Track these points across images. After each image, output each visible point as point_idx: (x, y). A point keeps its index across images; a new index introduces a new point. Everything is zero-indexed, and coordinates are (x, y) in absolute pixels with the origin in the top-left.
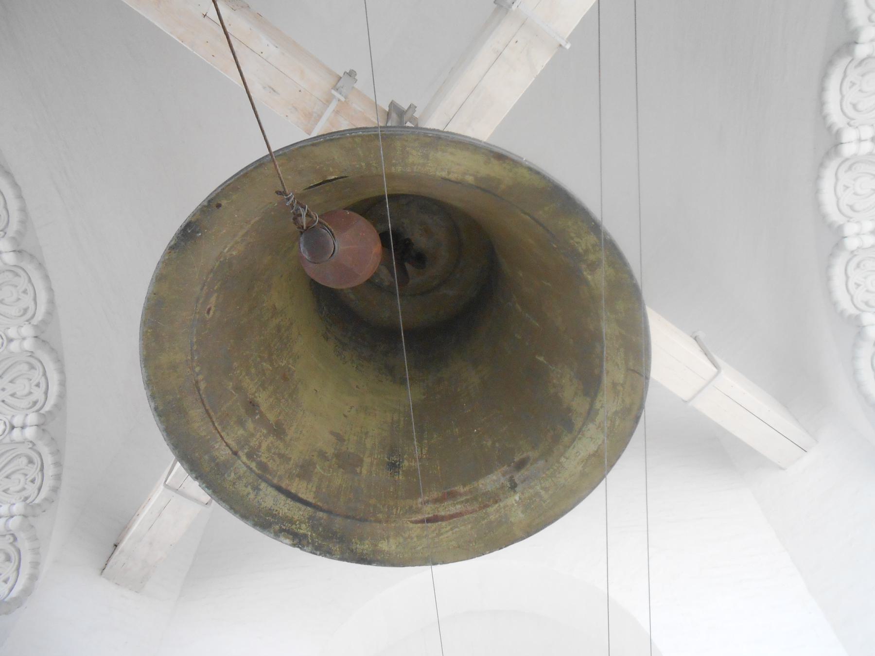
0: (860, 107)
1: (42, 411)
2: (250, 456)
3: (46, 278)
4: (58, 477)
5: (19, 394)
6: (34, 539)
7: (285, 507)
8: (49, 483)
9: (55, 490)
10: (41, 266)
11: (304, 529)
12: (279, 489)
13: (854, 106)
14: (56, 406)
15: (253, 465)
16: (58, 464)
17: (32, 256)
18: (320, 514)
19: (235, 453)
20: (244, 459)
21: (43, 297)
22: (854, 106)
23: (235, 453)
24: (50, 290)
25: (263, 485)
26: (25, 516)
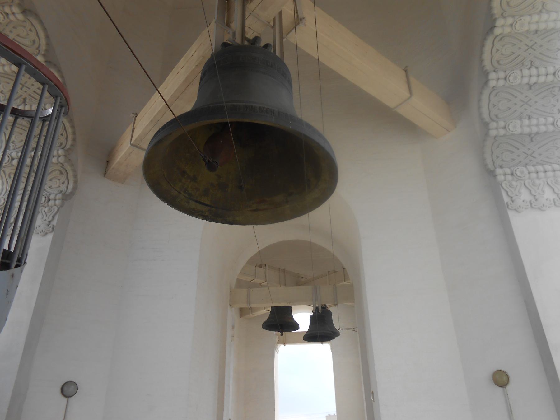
0: (501, 62)
1: (66, 149)
2: (185, 192)
3: (41, 22)
4: (74, 133)
5: (53, 186)
6: (72, 165)
7: (199, 207)
8: (70, 137)
9: (74, 140)
10: (37, 16)
11: (207, 214)
12: (197, 201)
13: (498, 62)
14: (72, 145)
15: (186, 195)
16: (73, 127)
17: (30, 11)
18: (213, 209)
19: (179, 192)
20: (183, 193)
21: (42, 34)
22: (498, 62)
23: (179, 192)
24: (45, 29)
25: (190, 201)
26: (65, 156)
